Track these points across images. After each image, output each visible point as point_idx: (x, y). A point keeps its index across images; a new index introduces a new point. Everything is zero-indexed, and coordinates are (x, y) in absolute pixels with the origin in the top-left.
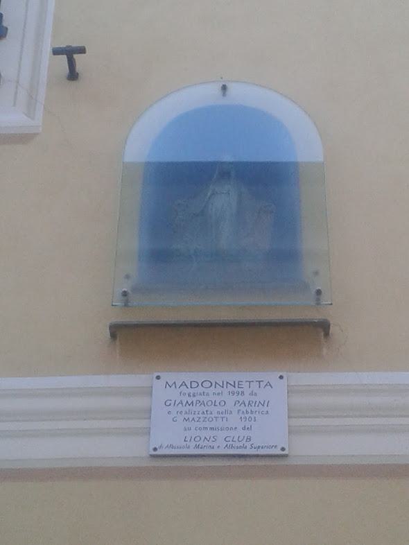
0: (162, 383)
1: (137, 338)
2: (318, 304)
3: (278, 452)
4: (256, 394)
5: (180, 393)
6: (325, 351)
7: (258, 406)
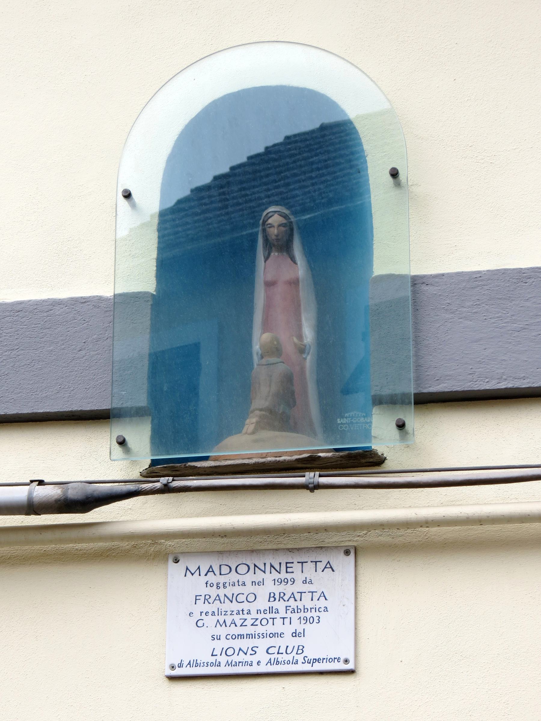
3: (341, 666)
4: (311, 582)
5: (207, 583)
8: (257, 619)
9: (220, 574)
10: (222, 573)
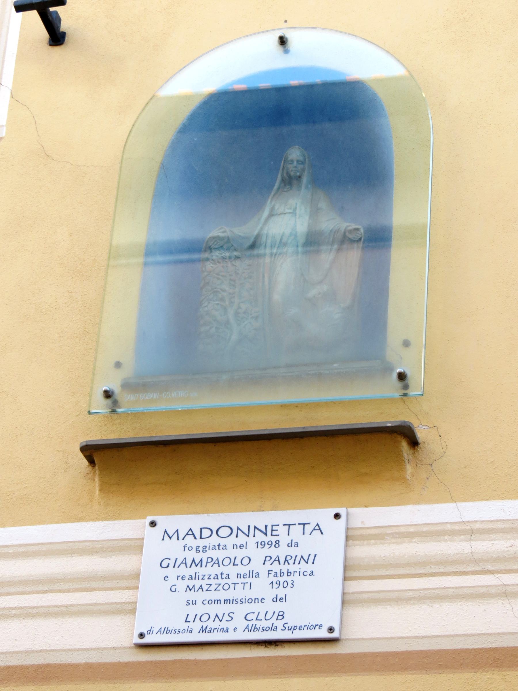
0: (159, 530)
1: (128, 462)
2: (405, 395)
3: (323, 634)
6: (409, 469)
7: (266, 526)
8: (220, 584)
9: (201, 538)
10: (202, 537)
